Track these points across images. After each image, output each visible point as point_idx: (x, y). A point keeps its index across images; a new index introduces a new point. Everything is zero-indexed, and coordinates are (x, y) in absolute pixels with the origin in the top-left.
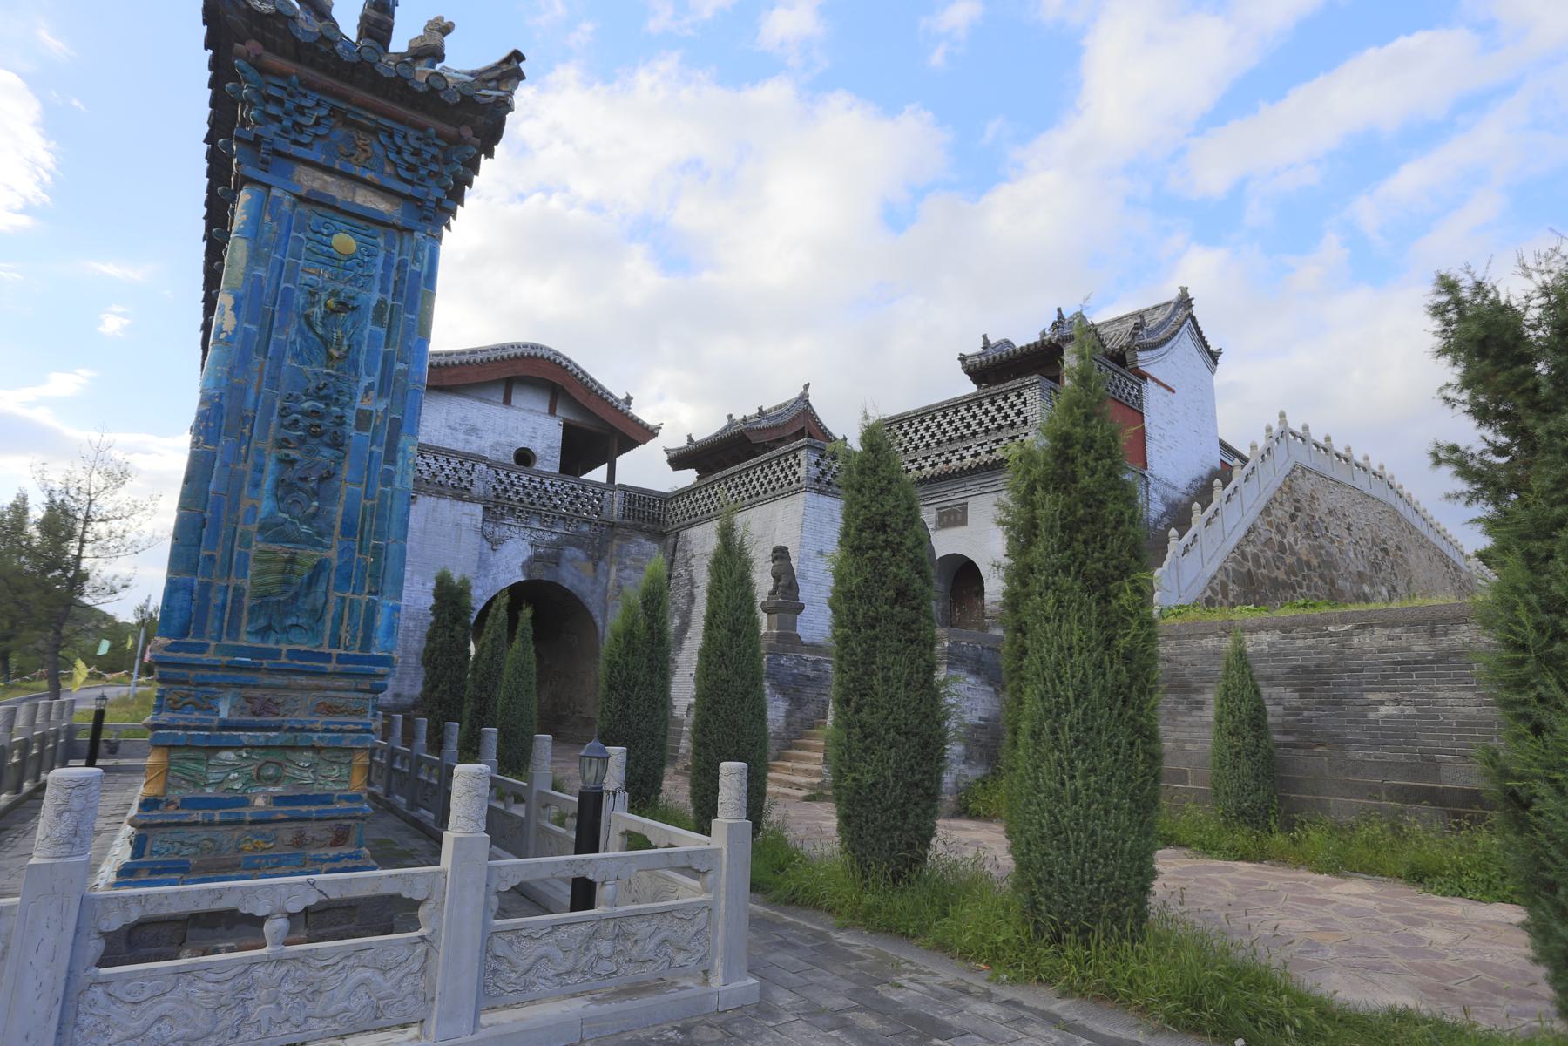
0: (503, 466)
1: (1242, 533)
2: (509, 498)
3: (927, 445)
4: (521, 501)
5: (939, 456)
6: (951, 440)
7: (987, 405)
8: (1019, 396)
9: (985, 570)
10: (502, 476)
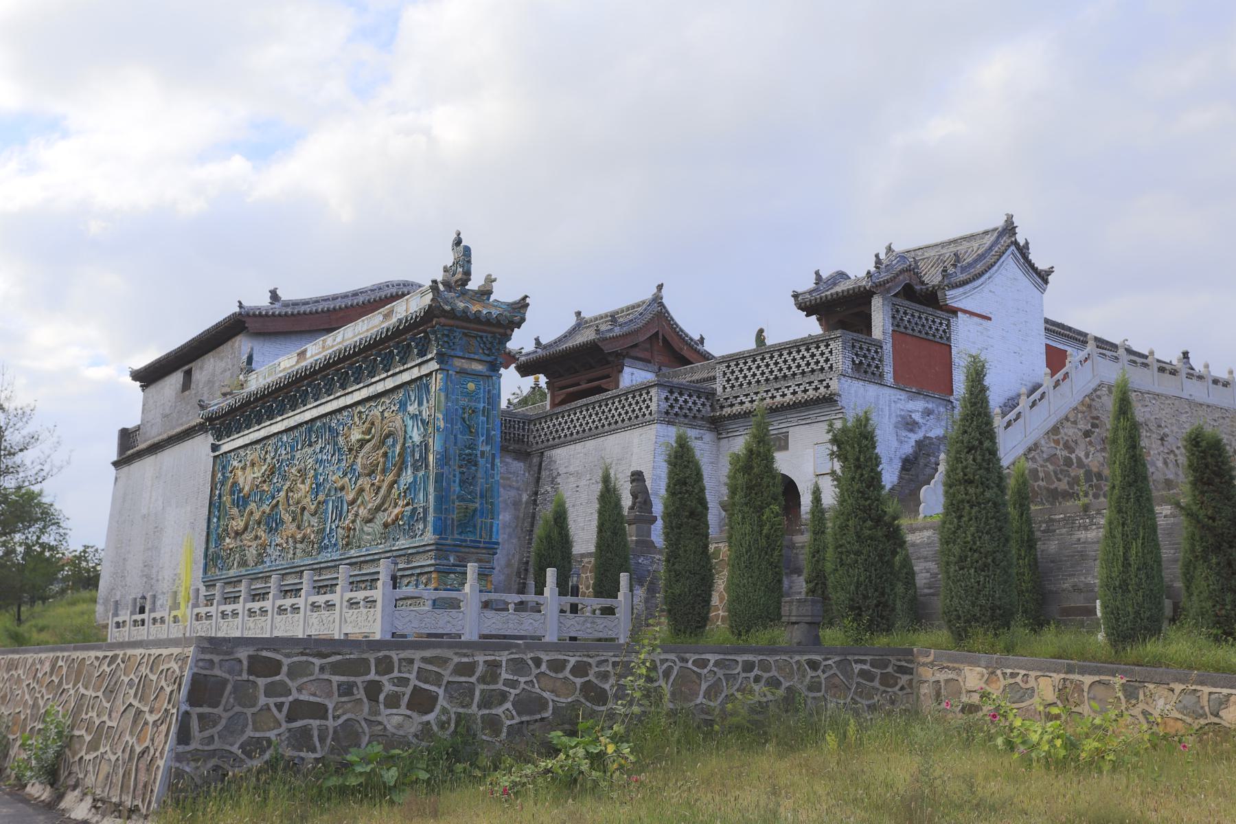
1: (1021, 451)
3: (758, 382)
5: (767, 392)
6: (776, 378)
7: (803, 352)
8: (827, 346)
9: (801, 487)
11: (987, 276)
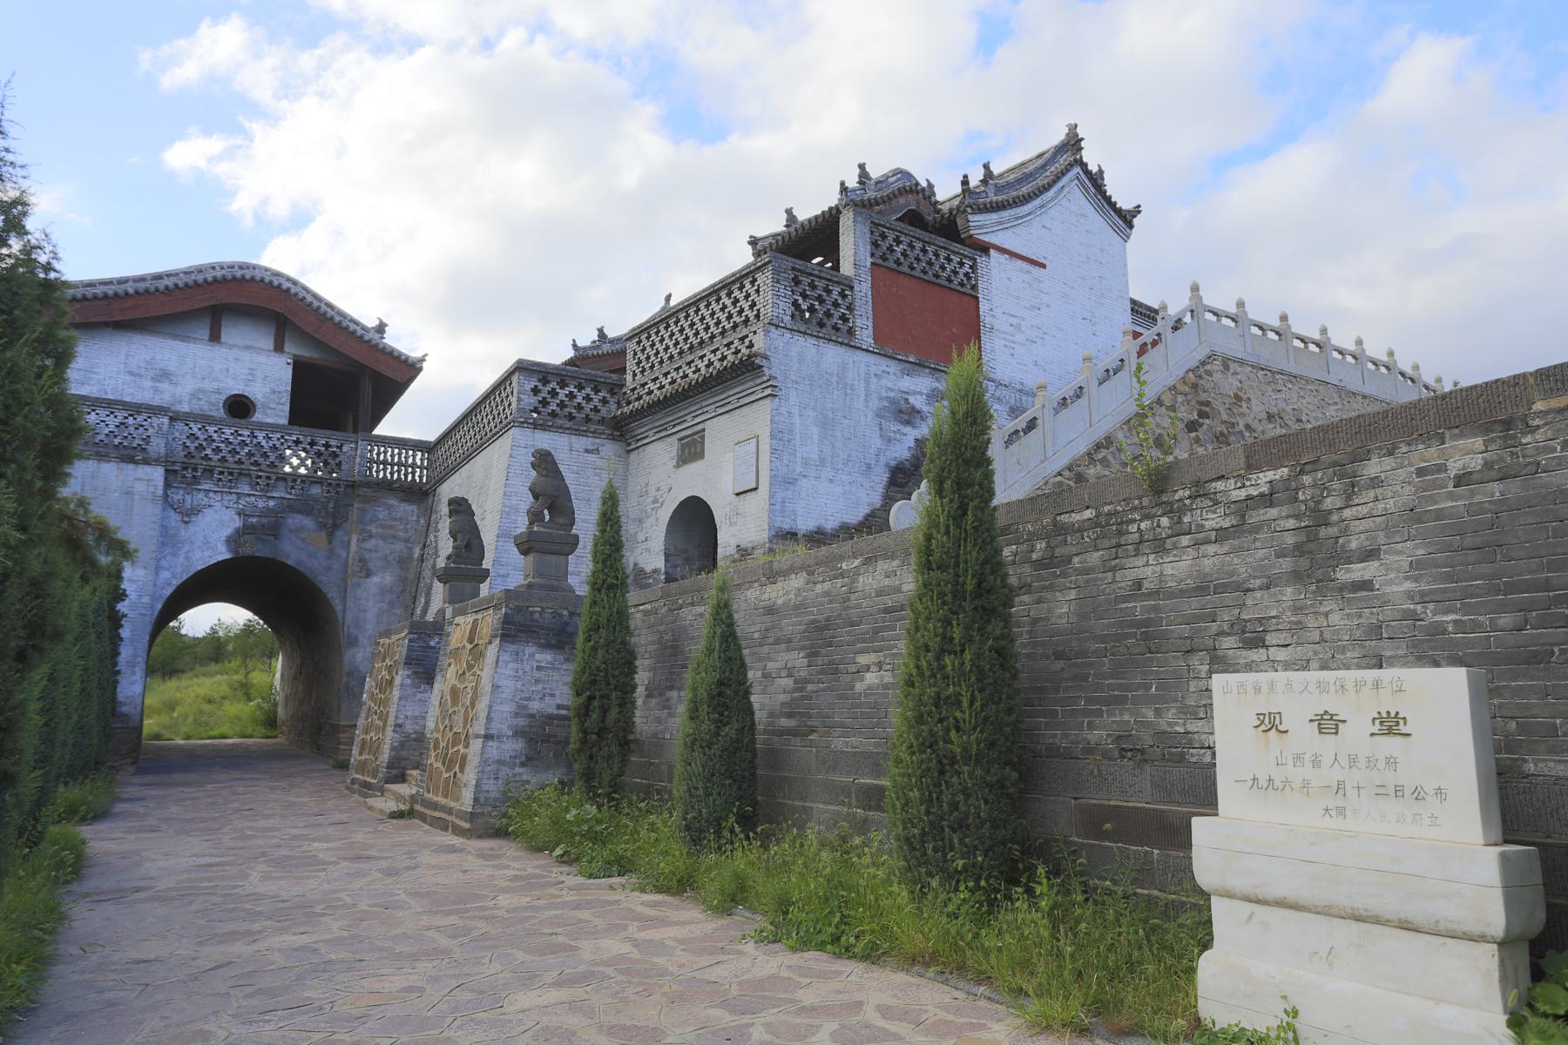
0: (206, 420)
2: (206, 457)
4: (224, 459)
10: (195, 430)
11: (1037, 202)
